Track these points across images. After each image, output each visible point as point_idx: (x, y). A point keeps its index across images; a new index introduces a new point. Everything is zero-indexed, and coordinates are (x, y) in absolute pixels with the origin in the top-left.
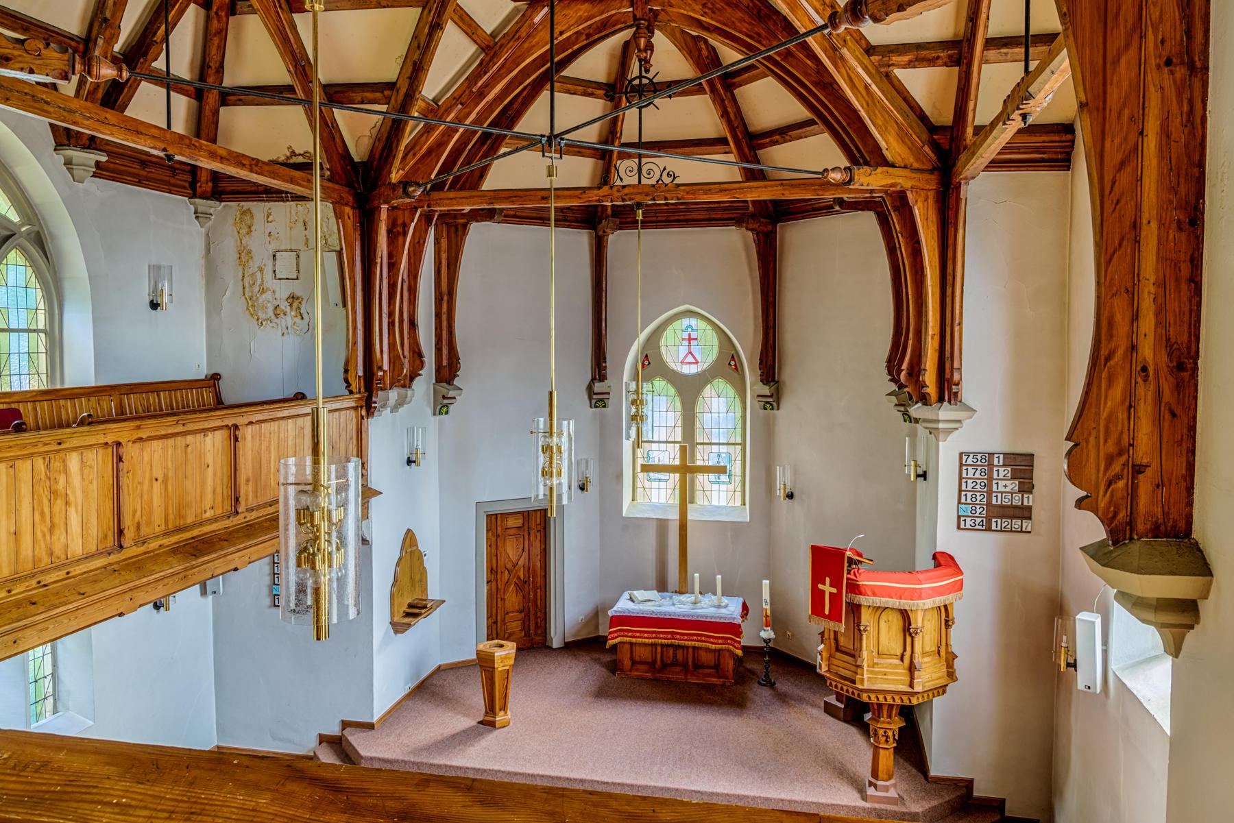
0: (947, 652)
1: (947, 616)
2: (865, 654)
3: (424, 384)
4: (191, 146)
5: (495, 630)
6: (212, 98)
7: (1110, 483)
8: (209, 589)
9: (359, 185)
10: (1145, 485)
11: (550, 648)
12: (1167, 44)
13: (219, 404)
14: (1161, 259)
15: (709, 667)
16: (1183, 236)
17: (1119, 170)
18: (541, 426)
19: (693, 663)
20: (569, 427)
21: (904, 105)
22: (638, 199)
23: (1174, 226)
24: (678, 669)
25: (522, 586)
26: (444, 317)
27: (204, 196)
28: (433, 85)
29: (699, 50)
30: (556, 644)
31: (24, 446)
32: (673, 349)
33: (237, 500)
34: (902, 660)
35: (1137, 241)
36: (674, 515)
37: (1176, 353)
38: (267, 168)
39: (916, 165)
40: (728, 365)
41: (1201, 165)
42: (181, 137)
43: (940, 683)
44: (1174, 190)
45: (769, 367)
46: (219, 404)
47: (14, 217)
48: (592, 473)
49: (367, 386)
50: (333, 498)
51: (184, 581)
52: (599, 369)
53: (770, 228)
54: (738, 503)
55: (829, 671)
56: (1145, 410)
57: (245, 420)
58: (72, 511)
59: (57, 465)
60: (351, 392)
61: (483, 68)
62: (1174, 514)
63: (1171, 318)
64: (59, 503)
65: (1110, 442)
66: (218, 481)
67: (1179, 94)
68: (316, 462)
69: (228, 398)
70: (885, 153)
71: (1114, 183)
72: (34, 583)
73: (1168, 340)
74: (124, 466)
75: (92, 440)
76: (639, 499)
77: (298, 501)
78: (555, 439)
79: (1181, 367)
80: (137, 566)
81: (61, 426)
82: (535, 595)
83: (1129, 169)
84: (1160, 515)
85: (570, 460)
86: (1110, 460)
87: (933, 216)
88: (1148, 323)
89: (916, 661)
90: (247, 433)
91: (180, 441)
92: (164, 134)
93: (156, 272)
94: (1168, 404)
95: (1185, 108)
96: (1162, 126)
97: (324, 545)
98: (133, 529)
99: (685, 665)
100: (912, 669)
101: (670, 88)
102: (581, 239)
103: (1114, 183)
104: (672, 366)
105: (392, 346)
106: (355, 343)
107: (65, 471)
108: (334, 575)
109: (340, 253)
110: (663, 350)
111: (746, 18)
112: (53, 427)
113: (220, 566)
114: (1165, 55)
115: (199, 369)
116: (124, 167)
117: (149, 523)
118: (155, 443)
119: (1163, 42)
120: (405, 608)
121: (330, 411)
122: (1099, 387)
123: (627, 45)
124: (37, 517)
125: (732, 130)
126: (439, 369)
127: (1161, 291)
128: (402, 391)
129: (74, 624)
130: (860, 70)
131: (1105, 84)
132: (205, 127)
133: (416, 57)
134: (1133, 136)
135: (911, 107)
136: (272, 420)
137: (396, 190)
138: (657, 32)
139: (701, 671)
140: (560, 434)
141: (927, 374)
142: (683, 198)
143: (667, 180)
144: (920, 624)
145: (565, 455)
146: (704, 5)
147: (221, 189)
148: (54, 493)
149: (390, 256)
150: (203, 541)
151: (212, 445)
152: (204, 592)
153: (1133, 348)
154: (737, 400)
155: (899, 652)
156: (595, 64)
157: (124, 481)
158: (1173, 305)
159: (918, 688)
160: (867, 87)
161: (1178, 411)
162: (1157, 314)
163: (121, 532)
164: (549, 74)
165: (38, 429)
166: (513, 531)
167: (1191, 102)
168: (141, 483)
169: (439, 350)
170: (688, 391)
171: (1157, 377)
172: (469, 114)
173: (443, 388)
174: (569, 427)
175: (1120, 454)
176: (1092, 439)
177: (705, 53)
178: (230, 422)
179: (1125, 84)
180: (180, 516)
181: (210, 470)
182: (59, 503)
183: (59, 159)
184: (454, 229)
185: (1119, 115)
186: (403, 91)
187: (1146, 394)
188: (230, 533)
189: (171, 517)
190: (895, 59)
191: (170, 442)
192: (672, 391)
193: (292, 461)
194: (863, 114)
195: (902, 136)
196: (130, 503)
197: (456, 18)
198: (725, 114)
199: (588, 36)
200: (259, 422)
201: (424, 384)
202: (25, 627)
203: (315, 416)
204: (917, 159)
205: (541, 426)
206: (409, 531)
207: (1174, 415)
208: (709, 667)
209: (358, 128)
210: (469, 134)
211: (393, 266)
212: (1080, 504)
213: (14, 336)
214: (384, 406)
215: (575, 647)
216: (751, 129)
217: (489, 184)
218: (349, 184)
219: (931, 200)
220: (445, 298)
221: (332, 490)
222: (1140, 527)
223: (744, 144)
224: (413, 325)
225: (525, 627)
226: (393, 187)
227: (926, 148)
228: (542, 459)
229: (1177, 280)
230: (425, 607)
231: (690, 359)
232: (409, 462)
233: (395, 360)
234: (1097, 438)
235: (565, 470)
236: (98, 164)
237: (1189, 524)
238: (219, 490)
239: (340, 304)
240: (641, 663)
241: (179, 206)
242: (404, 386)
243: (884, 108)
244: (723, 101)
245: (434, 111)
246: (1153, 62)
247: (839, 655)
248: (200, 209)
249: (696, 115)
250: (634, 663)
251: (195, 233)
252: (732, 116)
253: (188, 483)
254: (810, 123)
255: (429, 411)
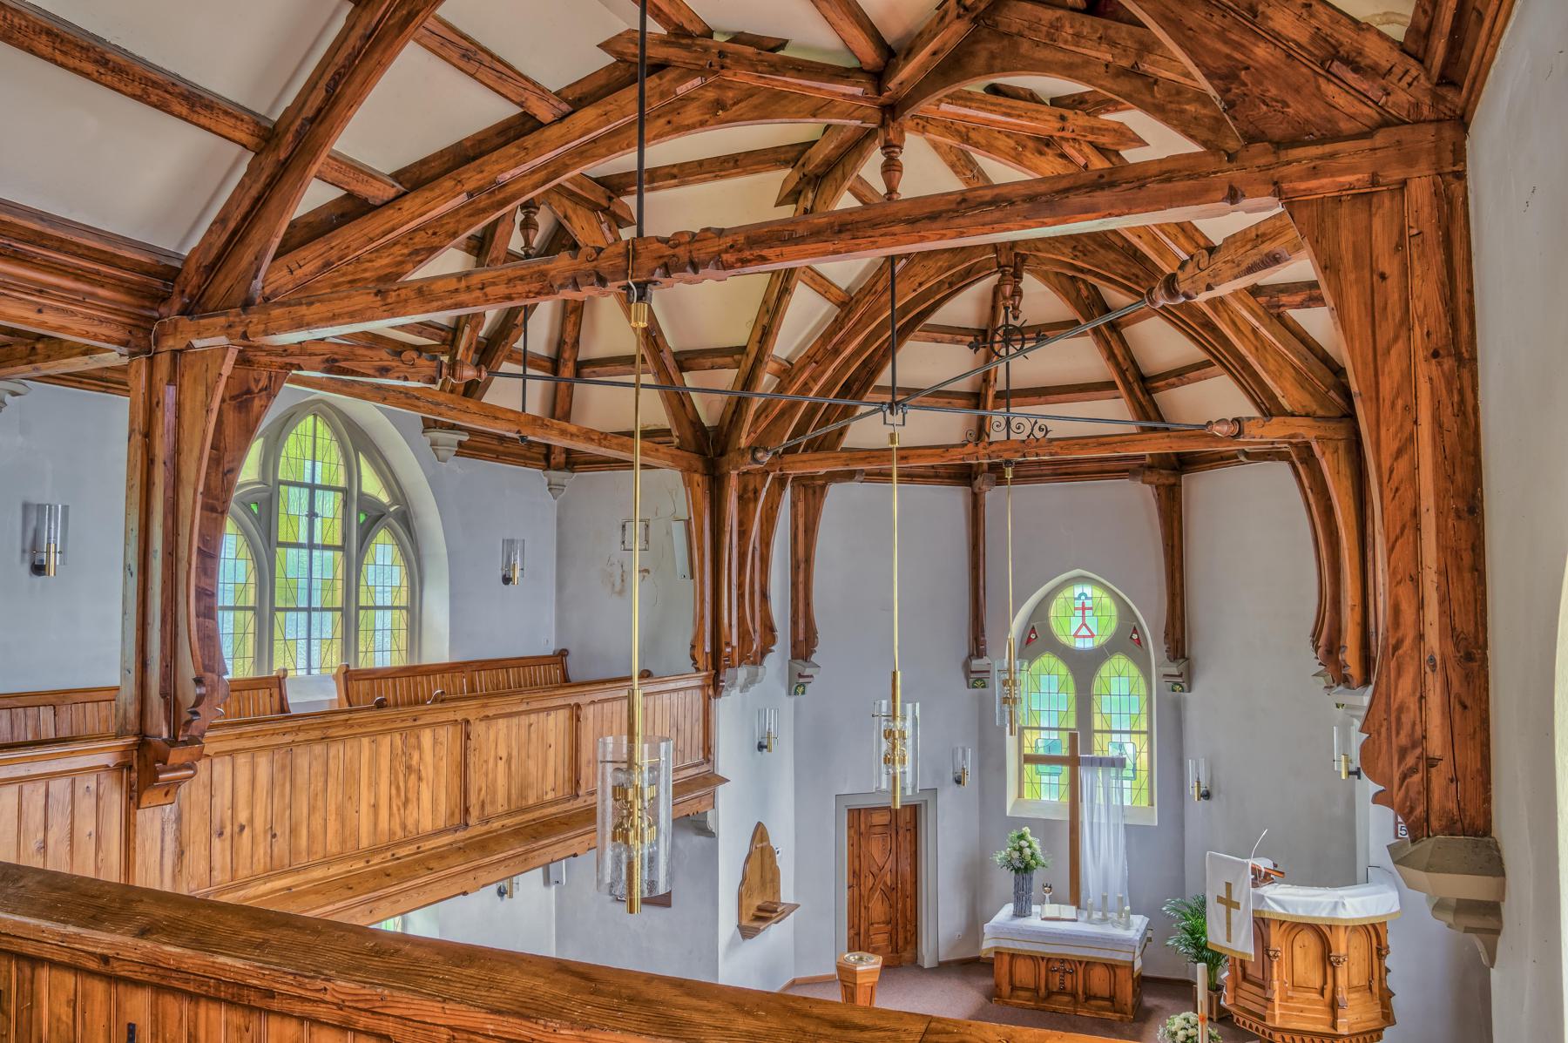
0: (1381, 988)
1: (1379, 943)
2: (1276, 984)
3: (777, 661)
4: (544, 426)
5: (858, 941)
6: (567, 371)
7: (1404, 777)
8: (553, 878)
9: (707, 450)
10: (1439, 778)
11: (921, 968)
12: (1433, 337)
13: (566, 681)
14: (1442, 547)
15: (1103, 999)
16: (1463, 525)
17: (1397, 458)
18: (884, 709)
19: (1084, 993)
20: (912, 710)
21: (1301, 347)
22: (1006, 456)
23: (1452, 514)
24: (1066, 999)
25: (890, 893)
26: (801, 587)
27: (558, 468)
28: (789, 341)
29: (1079, 291)
30: (927, 961)
31: (384, 722)
32: (1064, 621)
33: (578, 782)
34: (1322, 994)
35: (1418, 529)
36: (1065, 816)
37: (1463, 644)
38: (615, 441)
39: (1320, 412)
40: (1127, 641)
41: (1476, 453)
42: (535, 419)
43: (1373, 1025)
44: (1450, 478)
45: (1174, 640)
46: (566, 681)
47: (384, 498)
48: (970, 765)
49: (715, 665)
50: (646, 775)
51: (524, 863)
52: (978, 647)
53: (1172, 480)
54: (1145, 803)
55: (1235, 1004)
56: (1435, 699)
57: (588, 699)
58: (423, 786)
59: (413, 741)
60: (698, 670)
61: (838, 324)
62: (1471, 811)
63: (1455, 606)
64: (413, 777)
65: (1403, 733)
66: (560, 762)
67: (1449, 383)
68: (631, 741)
69: (574, 675)
70: (1284, 402)
71: (1391, 471)
72: (389, 854)
73: (1453, 629)
74: (472, 744)
75: (443, 717)
76: (1027, 795)
77: (615, 778)
78: (899, 723)
79: (1469, 657)
80: (482, 845)
81: (417, 703)
82: (904, 905)
83: (1406, 458)
84: (1455, 811)
85: (915, 749)
86: (1403, 752)
87: (1345, 469)
88: (1432, 612)
89: (1339, 997)
90: (589, 713)
91: (525, 720)
92: (520, 417)
93: (509, 544)
94: (1458, 696)
95: (1456, 398)
96: (1433, 416)
97: (637, 821)
98: (477, 807)
99: (1074, 995)
100: (1334, 1006)
101: (1042, 334)
102: (954, 499)
103: (1391, 471)
104: (1063, 639)
105: (742, 619)
106: (702, 617)
107: (419, 747)
108: (646, 852)
109: (688, 523)
110: (1053, 624)
111: (1122, 259)
112: (410, 704)
113: (558, 851)
114: (1432, 346)
115: (546, 645)
116: (479, 447)
117: (493, 802)
118: (500, 721)
119: (1428, 334)
120: (753, 911)
121: (645, 695)
122: (1388, 676)
123: (997, 290)
124: (394, 791)
125: (1122, 373)
126: (794, 645)
127: (1443, 579)
128: (752, 668)
129: (423, 899)
130: (1245, 313)
131: (1376, 375)
132: (560, 408)
133: (765, 321)
134: (1408, 426)
135: (1310, 349)
136: (614, 699)
137: (744, 455)
138: (1025, 275)
139: (1093, 1002)
140: (904, 719)
141: (1348, 652)
142: (1056, 454)
143: (1039, 435)
144: (1343, 951)
145: (909, 742)
146: (1074, 248)
147: (572, 462)
148: (409, 767)
149: (741, 523)
150: (544, 824)
151: (554, 725)
152: (547, 882)
153: (1421, 637)
154: (1142, 680)
155: (1318, 984)
156: (964, 308)
157: (472, 759)
158: (1456, 593)
159: (1343, 1030)
160: (1254, 331)
161: (1468, 703)
162: (1441, 602)
163: (467, 810)
164: (912, 322)
165: (396, 705)
166: (878, 830)
167: (1461, 392)
168: (486, 762)
169: (795, 623)
170: (1084, 666)
171: (1444, 668)
172: (823, 372)
173: (799, 666)
174: (912, 710)
175: (1414, 746)
176: (1384, 730)
177: (1084, 293)
178: (573, 701)
179: (1397, 375)
180: (522, 795)
181: (552, 750)
182: (413, 777)
183: (426, 440)
184: (812, 490)
185: (1393, 405)
186: (752, 355)
187: (1434, 685)
188: (570, 817)
189: (514, 797)
190: (1285, 299)
191: (515, 720)
192: (1062, 669)
193: (610, 740)
194: (1251, 359)
195: (1302, 380)
196: (476, 780)
197: (807, 280)
198: (1111, 356)
199: (951, 285)
200: (601, 701)
201: (777, 661)
202: (380, 898)
203: (630, 698)
204: (1322, 406)
205: (884, 709)
206: (759, 824)
207: (1465, 707)
208: (1103, 999)
209: (708, 395)
210: (813, 409)
211: (743, 534)
212: (1377, 799)
213: (379, 613)
214: (732, 685)
215: (944, 968)
216: (1144, 371)
217: (848, 441)
218: (700, 451)
219: (1341, 452)
220: (802, 566)
221: (646, 768)
222: (1435, 823)
223: (1136, 386)
224: (765, 596)
225: (893, 940)
226: (742, 452)
227: (1332, 394)
228: (885, 746)
229: (1459, 569)
230: (775, 911)
231: (1084, 632)
232: (761, 747)
233: (744, 635)
234: (1389, 729)
235: (909, 758)
236: (460, 444)
237: (1488, 822)
238: (560, 771)
239: (688, 575)
240: (1022, 989)
241: (533, 478)
242: (754, 663)
243: (1277, 352)
244: (1108, 343)
245: (787, 373)
246: (1421, 354)
247: (1246, 985)
248: (554, 481)
249: (1078, 357)
250: (1014, 988)
251: (548, 505)
252: (1120, 358)
253: (531, 764)
254: (1207, 364)
255: (784, 691)
